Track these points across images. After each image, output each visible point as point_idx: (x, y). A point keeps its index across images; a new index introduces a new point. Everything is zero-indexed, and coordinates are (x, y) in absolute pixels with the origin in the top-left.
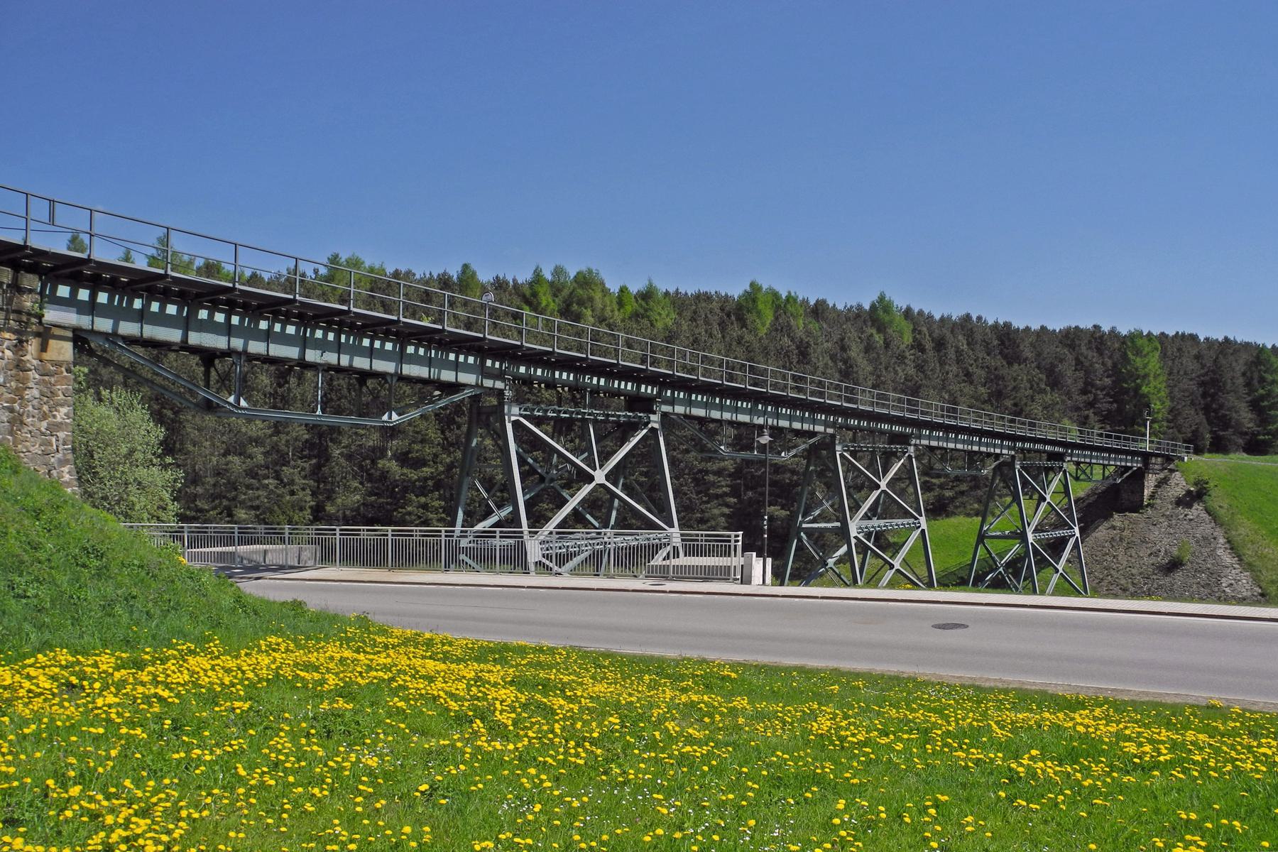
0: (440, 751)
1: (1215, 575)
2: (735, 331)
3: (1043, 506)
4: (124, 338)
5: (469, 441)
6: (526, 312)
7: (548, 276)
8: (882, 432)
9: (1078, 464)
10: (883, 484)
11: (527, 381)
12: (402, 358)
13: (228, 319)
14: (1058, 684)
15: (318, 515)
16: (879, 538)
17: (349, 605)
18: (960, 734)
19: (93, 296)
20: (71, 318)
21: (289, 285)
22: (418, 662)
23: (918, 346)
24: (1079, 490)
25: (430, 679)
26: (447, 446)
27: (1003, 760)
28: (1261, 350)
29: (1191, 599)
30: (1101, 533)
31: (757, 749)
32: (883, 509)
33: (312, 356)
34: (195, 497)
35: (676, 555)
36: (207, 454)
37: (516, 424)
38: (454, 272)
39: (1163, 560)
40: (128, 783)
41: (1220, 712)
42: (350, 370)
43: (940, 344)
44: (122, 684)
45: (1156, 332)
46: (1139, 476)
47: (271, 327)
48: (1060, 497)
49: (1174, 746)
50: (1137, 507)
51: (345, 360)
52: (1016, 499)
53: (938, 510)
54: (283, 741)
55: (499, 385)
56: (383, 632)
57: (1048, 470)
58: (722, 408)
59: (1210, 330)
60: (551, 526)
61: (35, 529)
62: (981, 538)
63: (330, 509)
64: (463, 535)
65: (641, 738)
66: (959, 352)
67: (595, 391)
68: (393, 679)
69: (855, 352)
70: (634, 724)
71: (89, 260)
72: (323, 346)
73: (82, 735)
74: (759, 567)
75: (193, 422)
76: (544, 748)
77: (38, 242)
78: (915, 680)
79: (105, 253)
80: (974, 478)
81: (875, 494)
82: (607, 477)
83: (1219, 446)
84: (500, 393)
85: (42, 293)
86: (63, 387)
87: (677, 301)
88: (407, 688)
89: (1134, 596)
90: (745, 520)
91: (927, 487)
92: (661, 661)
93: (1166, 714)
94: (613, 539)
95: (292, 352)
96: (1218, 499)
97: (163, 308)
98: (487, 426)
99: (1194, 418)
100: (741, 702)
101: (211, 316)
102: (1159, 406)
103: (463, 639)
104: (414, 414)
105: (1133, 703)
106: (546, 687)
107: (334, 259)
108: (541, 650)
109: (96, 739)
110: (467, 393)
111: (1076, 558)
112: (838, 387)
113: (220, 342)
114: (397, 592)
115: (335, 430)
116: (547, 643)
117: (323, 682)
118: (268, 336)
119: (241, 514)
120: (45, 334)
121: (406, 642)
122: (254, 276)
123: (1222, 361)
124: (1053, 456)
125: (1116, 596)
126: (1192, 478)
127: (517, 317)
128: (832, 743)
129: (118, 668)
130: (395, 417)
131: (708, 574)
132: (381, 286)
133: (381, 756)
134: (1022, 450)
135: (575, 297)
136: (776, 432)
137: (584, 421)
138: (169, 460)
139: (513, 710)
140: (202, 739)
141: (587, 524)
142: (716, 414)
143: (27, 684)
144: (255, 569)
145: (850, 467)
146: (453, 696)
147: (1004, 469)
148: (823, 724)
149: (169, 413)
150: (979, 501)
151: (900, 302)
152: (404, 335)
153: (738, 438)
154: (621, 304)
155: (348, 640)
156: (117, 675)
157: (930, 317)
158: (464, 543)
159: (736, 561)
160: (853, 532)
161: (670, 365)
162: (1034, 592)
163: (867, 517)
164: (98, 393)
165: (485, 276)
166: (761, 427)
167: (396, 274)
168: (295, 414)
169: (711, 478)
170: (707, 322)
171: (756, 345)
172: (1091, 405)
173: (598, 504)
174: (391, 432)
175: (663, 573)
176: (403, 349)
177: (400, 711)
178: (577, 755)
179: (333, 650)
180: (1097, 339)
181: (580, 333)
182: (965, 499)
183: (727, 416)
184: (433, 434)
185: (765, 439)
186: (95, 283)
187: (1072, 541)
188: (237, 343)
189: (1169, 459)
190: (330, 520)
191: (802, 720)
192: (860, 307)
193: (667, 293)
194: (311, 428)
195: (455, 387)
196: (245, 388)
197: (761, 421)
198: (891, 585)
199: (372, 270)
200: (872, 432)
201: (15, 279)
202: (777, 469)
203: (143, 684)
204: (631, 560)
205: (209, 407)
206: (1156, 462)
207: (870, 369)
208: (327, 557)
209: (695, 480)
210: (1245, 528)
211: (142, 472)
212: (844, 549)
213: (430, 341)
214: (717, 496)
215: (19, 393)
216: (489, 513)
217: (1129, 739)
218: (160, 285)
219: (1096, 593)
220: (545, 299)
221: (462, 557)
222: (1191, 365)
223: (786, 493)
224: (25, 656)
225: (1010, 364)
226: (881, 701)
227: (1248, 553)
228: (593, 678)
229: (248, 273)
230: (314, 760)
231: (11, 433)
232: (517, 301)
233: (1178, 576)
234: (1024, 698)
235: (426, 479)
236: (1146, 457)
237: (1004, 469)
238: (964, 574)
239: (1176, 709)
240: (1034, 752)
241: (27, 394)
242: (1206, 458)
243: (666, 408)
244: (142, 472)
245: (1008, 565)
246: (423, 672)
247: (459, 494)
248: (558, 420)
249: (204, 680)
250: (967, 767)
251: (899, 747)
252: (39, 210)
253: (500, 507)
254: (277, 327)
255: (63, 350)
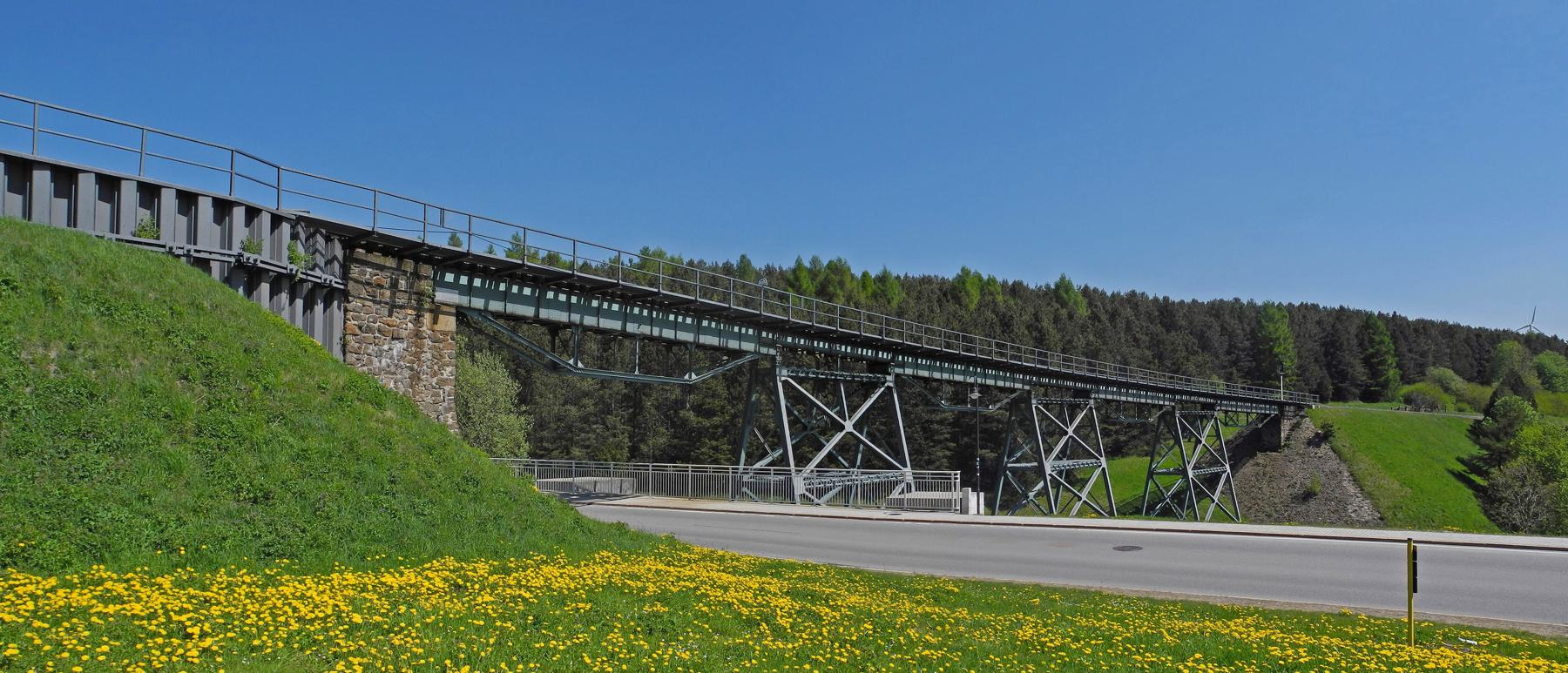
0: (736, 647)
1: (1342, 503)
2: (952, 307)
3: (1200, 447)
4: (492, 313)
5: (749, 395)
6: (791, 293)
7: (807, 264)
8: (1068, 389)
9: (1226, 412)
10: (1070, 431)
11: (793, 349)
12: (699, 330)
13: (569, 299)
14: (1216, 597)
15: (634, 453)
16: (1069, 475)
17: (658, 526)
18: (1137, 640)
19: (471, 281)
20: (453, 298)
21: (612, 271)
22: (714, 575)
23: (1095, 317)
24: (1228, 434)
25: (726, 589)
26: (732, 400)
27: (1173, 662)
28: (1369, 316)
29: (1323, 524)
30: (1248, 469)
31: (974, 651)
32: (1070, 452)
33: (631, 328)
34: (541, 440)
35: (909, 490)
36: (550, 404)
37: (785, 383)
38: (735, 262)
39: (1297, 490)
40: (503, 665)
41: (1351, 619)
42: (660, 339)
43: (1113, 316)
44: (494, 587)
45: (1285, 303)
46: (1276, 422)
47: (601, 305)
48: (1212, 440)
49: (1312, 650)
50: (1276, 447)
51: (656, 332)
52: (1178, 442)
53: (1115, 451)
54: (615, 636)
55: (772, 352)
56: (687, 550)
57: (1202, 418)
58: (941, 370)
59: (1329, 300)
60: (812, 465)
61: (429, 461)
62: (1151, 474)
63: (644, 448)
64: (746, 472)
65: (890, 642)
66: (1128, 323)
67: (845, 356)
68: (697, 588)
69: (1046, 323)
70: (883, 629)
71: (468, 254)
72: (639, 320)
73: (467, 625)
74: (975, 500)
75: (541, 378)
76: (814, 650)
77: (432, 240)
78: (1100, 593)
79: (479, 249)
80: (1144, 425)
81: (1065, 439)
82: (855, 426)
83: (1340, 396)
84: (773, 358)
85: (434, 279)
86: (448, 352)
87: (907, 284)
88: (707, 596)
89: (1278, 522)
90: (962, 461)
91: (1105, 433)
92: (899, 577)
93: (1307, 622)
94: (860, 477)
95: (616, 325)
96: (1340, 439)
97: (521, 290)
98: (763, 384)
99: (1318, 373)
100: (963, 613)
101: (556, 296)
102: (1290, 363)
103: (748, 556)
104: (707, 375)
105: (1278, 612)
106: (814, 597)
107: (645, 251)
108: (807, 567)
109: (478, 629)
110: (748, 358)
111: (1228, 489)
112: (1033, 353)
113: (562, 317)
114: (695, 517)
115: (646, 385)
116: (811, 561)
117: (644, 589)
118: (598, 312)
119: (576, 451)
120: (436, 311)
121: (704, 558)
122: (585, 264)
123: (1338, 326)
124: (1205, 406)
125: (1262, 522)
126: (1319, 423)
127: (783, 297)
128: (1034, 648)
129: (491, 574)
130: (694, 376)
131: (934, 506)
132: (681, 273)
133: (691, 650)
134: (1181, 401)
135: (828, 281)
136: (984, 389)
137: (837, 382)
138: (524, 408)
139: (790, 616)
140: (556, 632)
141: (839, 465)
142: (937, 375)
143: (426, 584)
144: (588, 496)
145: (1043, 417)
146: (742, 602)
147: (1166, 418)
148: (1027, 632)
149: (523, 372)
150: (1148, 444)
151: (1078, 282)
152: (700, 312)
153: (956, 393)
154: (864, 287)
155: (661, 555)
156: (491, 579)
157: (1103, 294)
158: (746, 478)
159: (955, 495)
160: (1048, 470)
161: (901, 335)
162: (1196, 519)
163: (1058, 458)
164: (472, 356)
165: (758, 264)
166: (972, 385)
167: (691, 263)
168: (619, 374)
169: (936, 426)
170: (930, 301)
171: (967, 318)
172: (1234, 363)
173: (847, 448)
174: (689, 389)
175: (899, 505)
176: (699, 323)
177: (704, 614)
178: (841, 654)
179: (650, 563)
180: (1236, 308)
181: (832, 310)
182: (1137, 442)
183: (946, 376)
184: (721, 389)
185: (976, 395)
186: (472, 271)
187: (1224, 476)
188: (576, 318)
189: (1300, 407)
190: (643, 457)
191: (1010, 628)
192: (1048, 286)
193: (898, 278)
194: (628, 384)
195: (738, 353)
196: (579, 353)
197: (972, 380)
198: (1080, 514)
199: (672, 259)
200: (1060, 388)
201: (416, 268)
202: (987, 419)
203: (510, 587)
204: (874, 494)
205: (554, 367)
206: (1290, 410)
207: (1059, 336)
208: (642, 488)
209: (924, 429)
210: (1364, 464)
211: (503, 418)
212: (1041, 484)
213: (720, 317)
214: (940, 442)
215: (417, 355)
216: (764, 455)
217: (1274, 643)
218: (519, 272)
219: (1247, 520)
220: (806, 283)
221: (745, 489)
222: (1315, 330)
223: (994, 438)
224: (424, 562)
225: (1168, 331)
226: (1073, 612)
227: (1368, 484)
228: (848, 590)
229: (580, 262)
230: (640, 652)
231: (411, 386)
232: (782, 284)
233: (1312, 503)
234: (1190, 609)
235: (716, 427)
236: (1281, 405)
237: (1166, 418)
238: (1138, 504)
239: (1314, 617)
240: (1198, 656)
241: (424, 357)
242: (1331, 406)
243: (898, 371)
244: (503, 418)
245: (1173, 496)
246: (719, 583)
247: (742, 439)
248: (816, 380)
249: (556, 585)
250: (1143, 669)
251: (1088, 651)
252: (433, 216)
253: (773, 450)
254: (605, 306)
255: (448, 323)
